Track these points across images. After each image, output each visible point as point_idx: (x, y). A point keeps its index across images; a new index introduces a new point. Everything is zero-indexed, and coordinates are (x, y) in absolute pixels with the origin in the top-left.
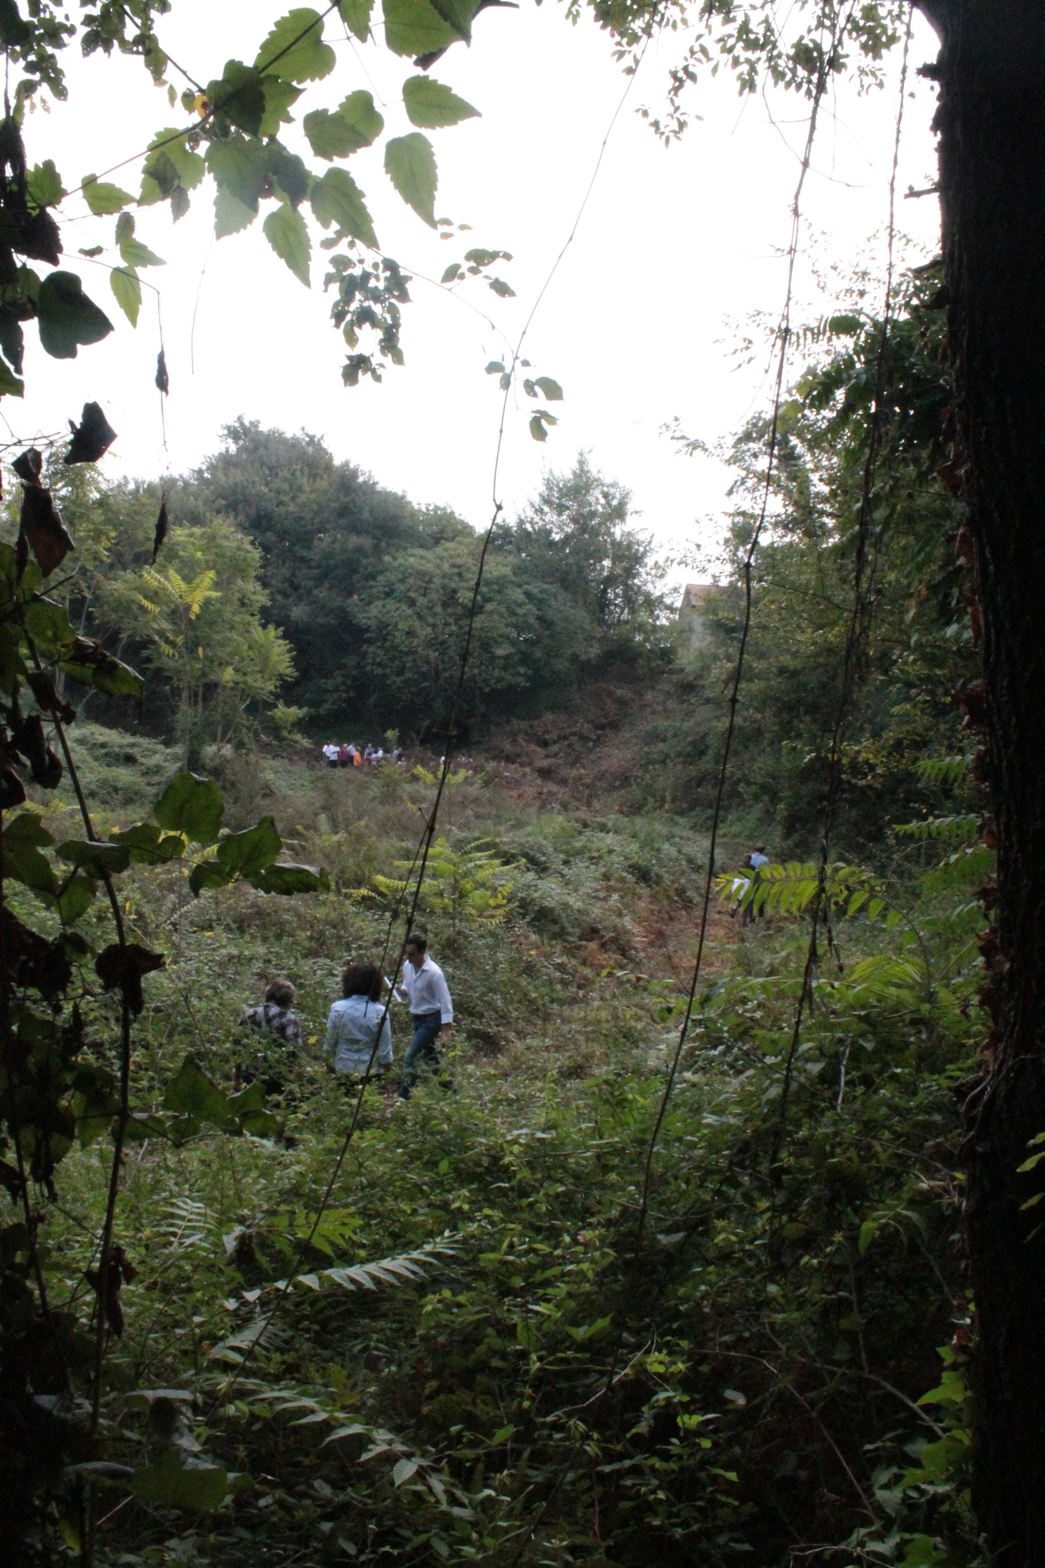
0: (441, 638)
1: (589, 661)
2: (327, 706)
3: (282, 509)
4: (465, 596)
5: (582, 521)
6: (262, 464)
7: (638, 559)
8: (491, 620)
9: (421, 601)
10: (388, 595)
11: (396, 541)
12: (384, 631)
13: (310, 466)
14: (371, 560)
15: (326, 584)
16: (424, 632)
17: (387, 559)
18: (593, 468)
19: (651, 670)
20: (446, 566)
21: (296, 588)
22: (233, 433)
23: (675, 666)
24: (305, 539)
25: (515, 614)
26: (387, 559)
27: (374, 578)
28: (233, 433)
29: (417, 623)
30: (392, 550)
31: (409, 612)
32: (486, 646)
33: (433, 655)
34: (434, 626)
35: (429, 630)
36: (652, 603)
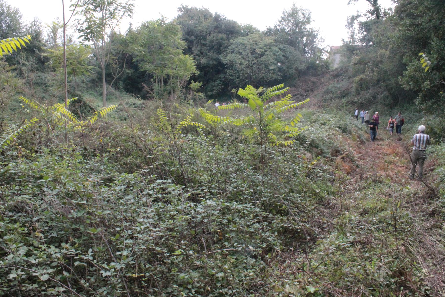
0: (251, 65)
1: (301, 70)
2: (214, 91)
3: (197, 29)
4: (258, 51)
5: (297, 24)
6: (189, 16)
7: (315, 37)
8: (269, 58)
9: (244, 53)
10: (233, 52)
11: (234, 35)
12: (232, 64)
13: (205, 16)
14: (226, 41)
15: (212, 51)
16: (245, 63)
17: (231, 40)
18: (298, 6)
19: (323, 72)
20: (251, 41)
21: (202, 54)
22: (180, 10)
23: (331, 69)
24: (204, 38)
25: (276, 55)
26: (231, 40)
27: (228, 48)
28: (180, 10)
29: (243, 61)
30: (233, 38)
31: (240, 57)
32: (266, 66)
33: (249, 71)
34: (249, 61)
35: (247, 62)
36: (320, 51)
